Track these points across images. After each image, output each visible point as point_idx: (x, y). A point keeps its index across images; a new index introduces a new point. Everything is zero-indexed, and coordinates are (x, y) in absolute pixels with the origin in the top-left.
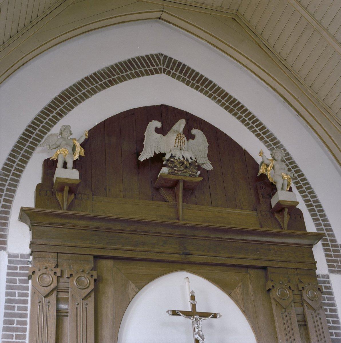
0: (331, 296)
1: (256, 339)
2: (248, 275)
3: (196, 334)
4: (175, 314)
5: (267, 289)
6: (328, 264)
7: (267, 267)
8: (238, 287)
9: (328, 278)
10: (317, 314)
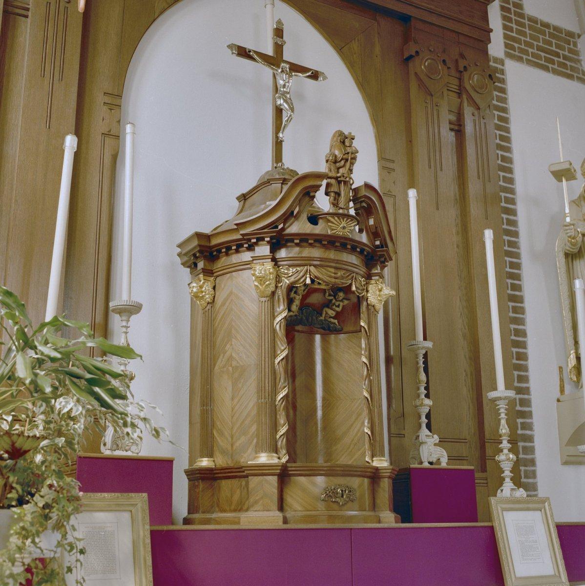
0: (503, 95)
1: (375, 136)
2: (376, 24)
3: (279, 98)
4: (244, 54)
5: (406, 55)
6: (504, 42)
7: (411, 16)
8: (356, 40)
9: (503, 65)
10: (481, 117)
